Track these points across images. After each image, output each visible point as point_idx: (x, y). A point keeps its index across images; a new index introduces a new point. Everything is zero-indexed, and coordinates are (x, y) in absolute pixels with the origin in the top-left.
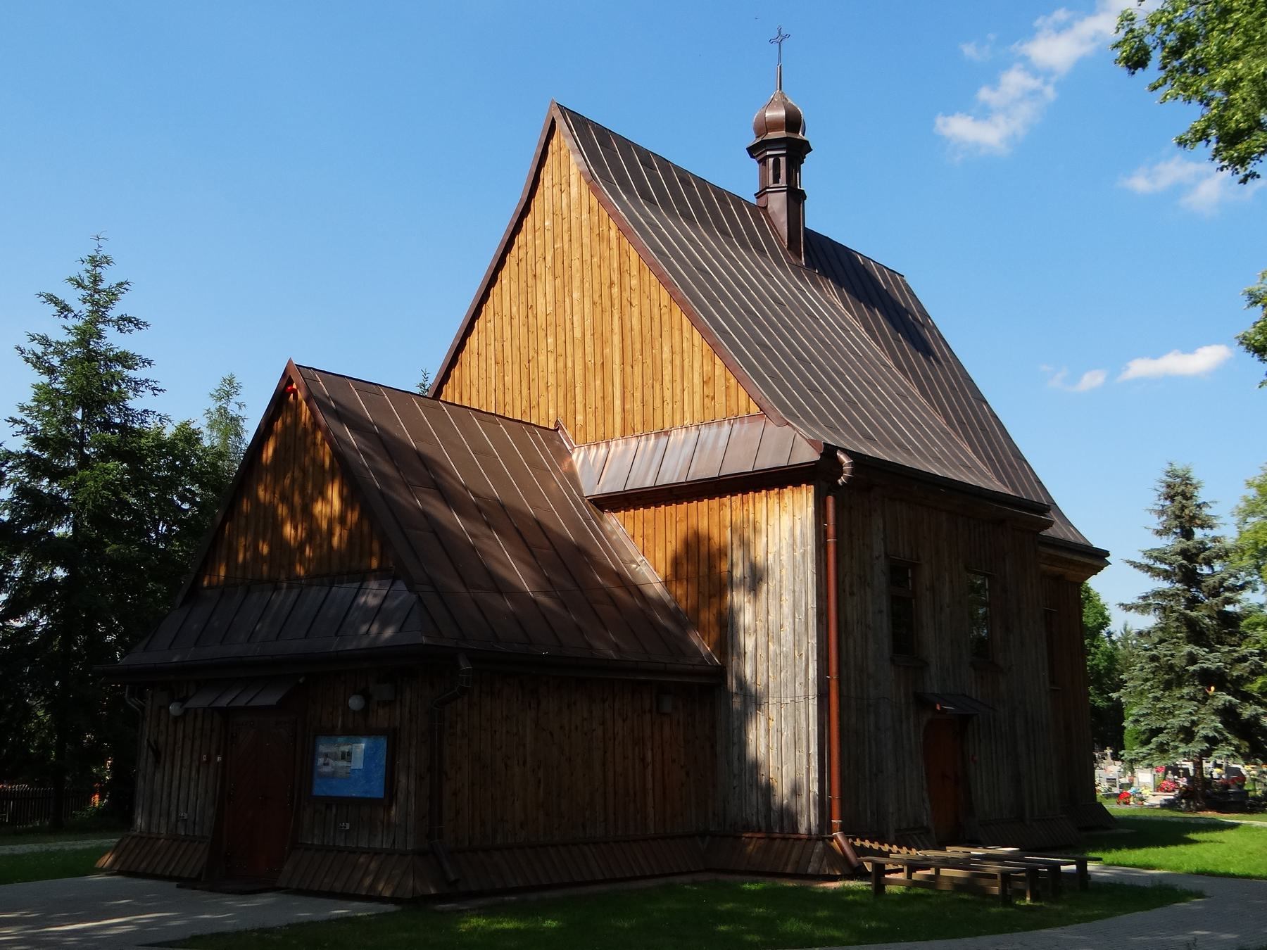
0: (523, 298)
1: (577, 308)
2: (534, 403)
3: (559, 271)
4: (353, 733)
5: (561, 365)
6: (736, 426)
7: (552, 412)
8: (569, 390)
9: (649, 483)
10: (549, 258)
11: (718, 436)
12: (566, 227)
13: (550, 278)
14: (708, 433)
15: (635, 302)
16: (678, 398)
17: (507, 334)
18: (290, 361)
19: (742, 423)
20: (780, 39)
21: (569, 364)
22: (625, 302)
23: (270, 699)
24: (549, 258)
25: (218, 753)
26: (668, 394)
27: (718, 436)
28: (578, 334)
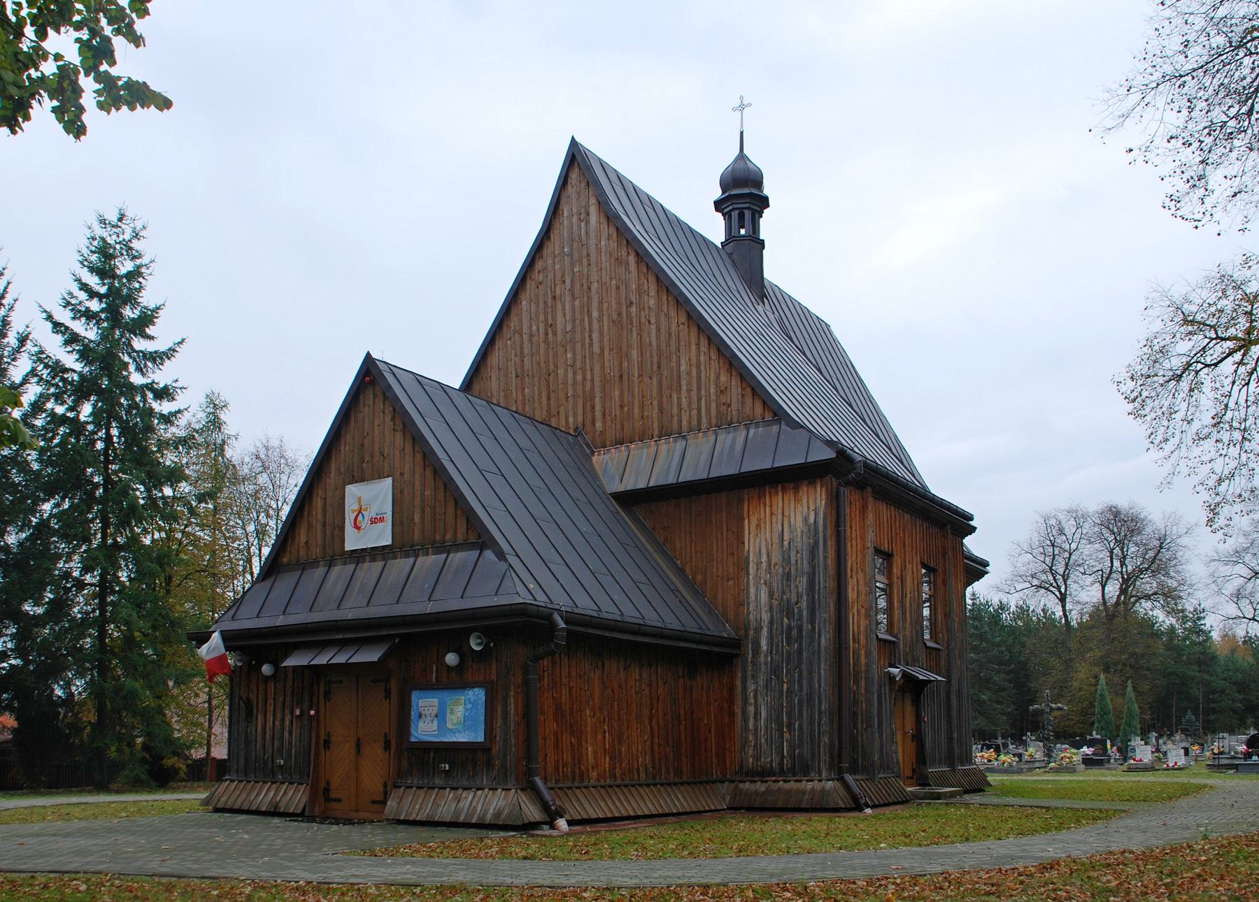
0: (542, 317)
1: (595, 326)
2: (554, 411)
3: (577, 294)
4: (455, 681)
5: (579, 377)
6: (752, 431)
7: (571, 420)
8: (589, 399)
9: (671, 480)
10: (568, 281)
11: (734, 440)
12: (585, 253)
13: (568, 299)
14: (725, 438)
15: (653, 320)
16: (695, 406)
17: (526, 351)
18: (368, 355)
19: (757, 427)
20: (742, 107)
21: (589, 377)
22: (643, 320)
23: (371, 655)
24: (568, 281)
25: (311, 708)
26: (684, 402)
27: (734, 440)
28: (596, 349)
